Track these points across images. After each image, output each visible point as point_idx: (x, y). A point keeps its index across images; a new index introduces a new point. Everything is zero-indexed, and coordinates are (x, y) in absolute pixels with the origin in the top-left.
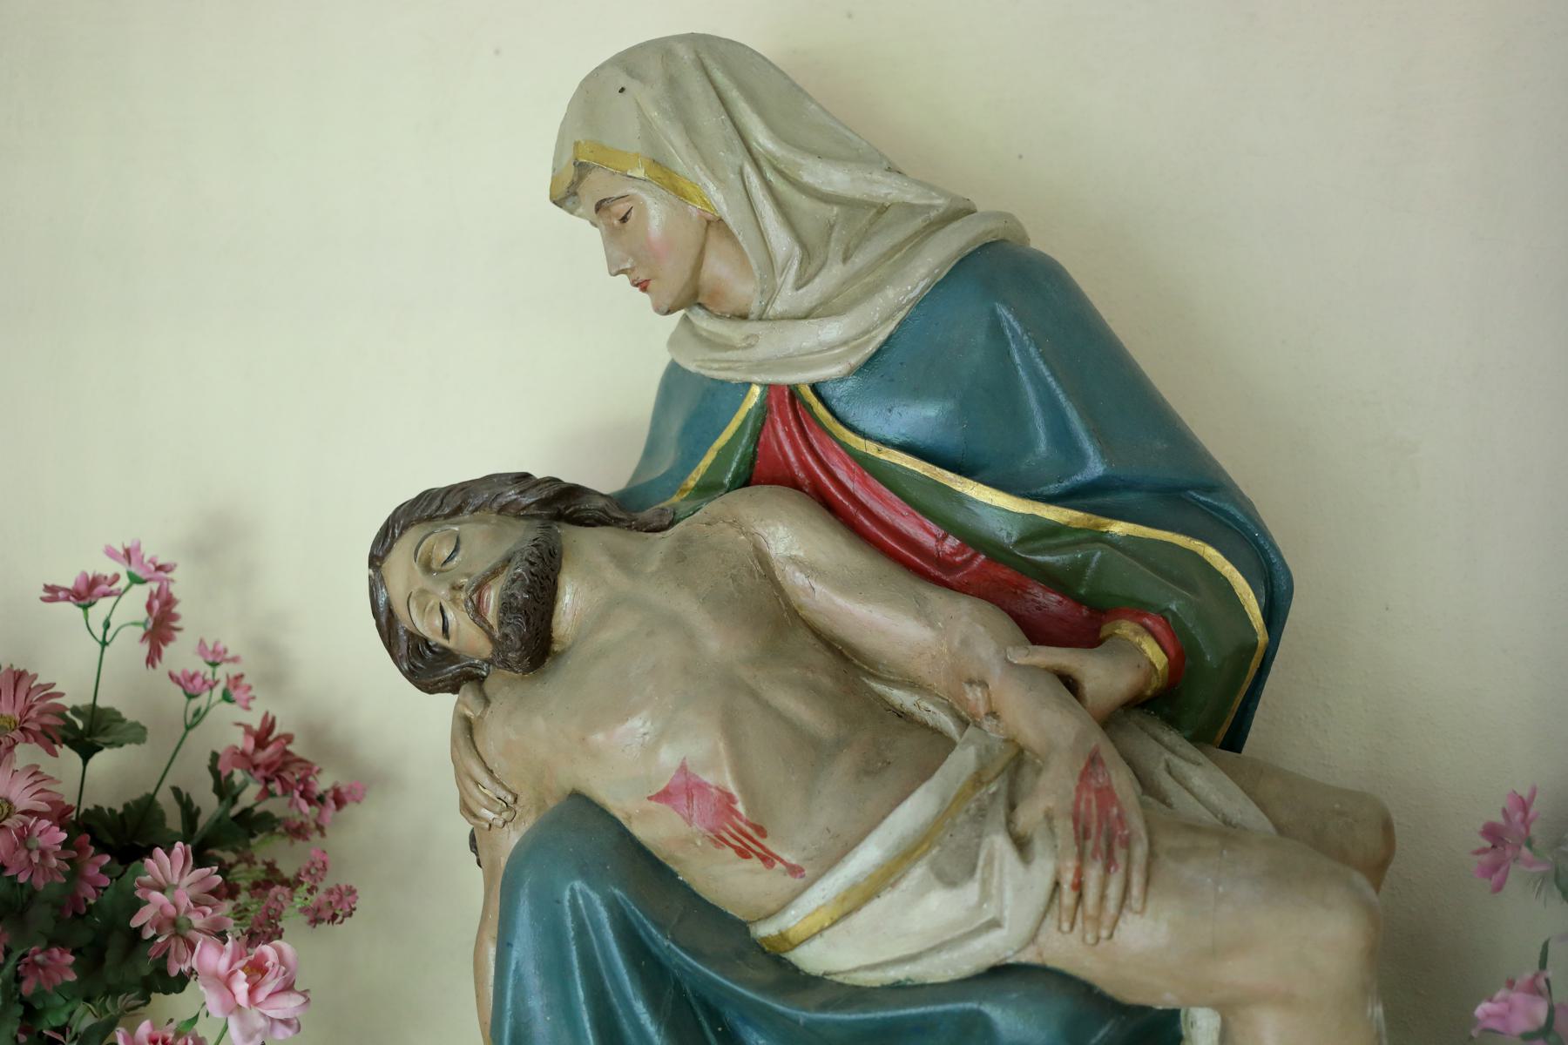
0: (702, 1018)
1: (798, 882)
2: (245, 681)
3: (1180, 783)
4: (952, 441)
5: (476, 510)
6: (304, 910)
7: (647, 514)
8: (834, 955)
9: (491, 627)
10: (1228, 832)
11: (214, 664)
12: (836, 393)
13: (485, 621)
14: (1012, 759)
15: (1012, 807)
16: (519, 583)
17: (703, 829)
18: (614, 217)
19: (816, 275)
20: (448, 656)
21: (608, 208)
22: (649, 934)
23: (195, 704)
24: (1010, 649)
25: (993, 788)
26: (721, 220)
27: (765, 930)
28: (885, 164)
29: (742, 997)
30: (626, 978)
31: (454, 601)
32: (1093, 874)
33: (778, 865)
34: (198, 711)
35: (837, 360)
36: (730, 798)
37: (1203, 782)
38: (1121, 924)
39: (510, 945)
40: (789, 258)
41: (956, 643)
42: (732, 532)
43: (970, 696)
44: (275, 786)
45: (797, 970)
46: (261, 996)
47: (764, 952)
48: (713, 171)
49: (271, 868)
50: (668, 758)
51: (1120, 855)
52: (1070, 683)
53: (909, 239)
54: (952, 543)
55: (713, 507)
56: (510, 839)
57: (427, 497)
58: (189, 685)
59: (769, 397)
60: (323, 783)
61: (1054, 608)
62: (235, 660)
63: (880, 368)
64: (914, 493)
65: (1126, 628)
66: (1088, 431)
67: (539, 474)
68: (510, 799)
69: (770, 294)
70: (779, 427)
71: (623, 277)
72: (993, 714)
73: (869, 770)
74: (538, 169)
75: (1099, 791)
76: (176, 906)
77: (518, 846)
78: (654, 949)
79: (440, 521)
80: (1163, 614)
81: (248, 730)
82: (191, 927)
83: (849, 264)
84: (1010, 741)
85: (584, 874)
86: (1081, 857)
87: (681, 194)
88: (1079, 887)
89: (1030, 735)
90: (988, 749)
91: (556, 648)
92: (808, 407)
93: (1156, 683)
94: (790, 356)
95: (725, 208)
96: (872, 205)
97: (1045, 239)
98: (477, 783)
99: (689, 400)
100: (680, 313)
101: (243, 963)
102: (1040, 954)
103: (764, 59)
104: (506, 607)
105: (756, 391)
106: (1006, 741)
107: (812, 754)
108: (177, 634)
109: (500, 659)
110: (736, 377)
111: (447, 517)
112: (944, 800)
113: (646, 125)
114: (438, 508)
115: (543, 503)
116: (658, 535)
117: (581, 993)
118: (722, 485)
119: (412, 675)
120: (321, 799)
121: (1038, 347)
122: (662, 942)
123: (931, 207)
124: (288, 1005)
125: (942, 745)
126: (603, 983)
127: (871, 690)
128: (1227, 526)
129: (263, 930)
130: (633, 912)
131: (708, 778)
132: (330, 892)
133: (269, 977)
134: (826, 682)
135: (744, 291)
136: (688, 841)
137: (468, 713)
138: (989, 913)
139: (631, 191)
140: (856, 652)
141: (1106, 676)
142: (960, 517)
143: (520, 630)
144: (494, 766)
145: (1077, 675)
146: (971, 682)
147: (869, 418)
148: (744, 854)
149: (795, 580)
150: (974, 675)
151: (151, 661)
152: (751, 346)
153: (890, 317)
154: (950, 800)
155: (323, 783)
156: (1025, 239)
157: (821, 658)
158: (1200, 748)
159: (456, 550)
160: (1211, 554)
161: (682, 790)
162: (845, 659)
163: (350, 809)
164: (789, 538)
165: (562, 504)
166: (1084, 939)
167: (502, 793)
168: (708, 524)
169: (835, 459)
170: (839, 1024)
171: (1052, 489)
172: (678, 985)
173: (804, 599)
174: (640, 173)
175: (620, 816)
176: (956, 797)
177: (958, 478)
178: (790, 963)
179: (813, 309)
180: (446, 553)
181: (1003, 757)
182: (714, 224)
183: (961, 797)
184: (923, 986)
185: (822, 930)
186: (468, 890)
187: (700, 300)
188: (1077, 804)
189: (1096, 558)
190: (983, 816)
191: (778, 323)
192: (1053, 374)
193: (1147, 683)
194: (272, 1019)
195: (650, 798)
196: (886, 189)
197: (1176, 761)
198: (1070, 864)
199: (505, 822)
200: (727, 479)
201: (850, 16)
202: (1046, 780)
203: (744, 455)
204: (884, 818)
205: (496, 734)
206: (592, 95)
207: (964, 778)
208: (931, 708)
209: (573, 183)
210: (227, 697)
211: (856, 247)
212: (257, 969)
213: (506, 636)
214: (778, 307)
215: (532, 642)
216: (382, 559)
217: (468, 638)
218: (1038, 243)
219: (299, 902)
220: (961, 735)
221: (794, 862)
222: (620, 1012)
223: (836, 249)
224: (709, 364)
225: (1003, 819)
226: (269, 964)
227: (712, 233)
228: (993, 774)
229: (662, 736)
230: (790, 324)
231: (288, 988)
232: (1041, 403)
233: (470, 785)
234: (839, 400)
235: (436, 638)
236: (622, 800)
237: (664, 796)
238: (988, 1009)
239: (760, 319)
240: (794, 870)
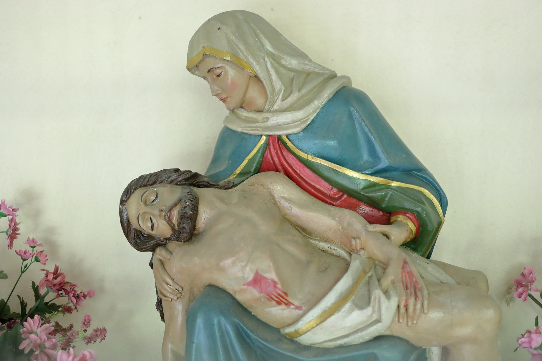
1: (301, 312)
2: (44, 253)
4: (335, 154)
6: (84, 338)
8: (317, 337)
9: (174, 225)
11: (33, 247)
13: (172, 223)
18: (213, 75)
20: (150, 237)
21: (213, 71)
23: (25, 263)
27: (288, 330)
32: (411, 301)
34: (27, 265)
35: (297, 126)
40: (280, 90)
45: (300, 344)
51: (419, 294)
52: (387, 236)
55: (252, 179)
57: (142, 178)
58: (24, 256)
59: (269, 140)
62: (40, 245)
63: (309, 129)
65: (401, 218)
67: (182, 169)
68: (180, 289)
70: (272, 150)
75: (408, 273)
76: (40, 339)
82: (45, 348)
84: (370, 258)
85: (222, 313)
86: (407, 295)
93: (412, 236)
98: (167, 284)
99: (230, 141)
102: (391, 331)
105: (264, 138)
108: (18, 236)
111: (150, 185)
113: (229, 41)
115: (186, 180)
118: (250, 172)
144: (175, 277)
148: (279, 303)
149: (285, 204)
151: (10, 246)
152: (264, 122)
153: (315, 112)
159: (157, 197)
160: (426, 192)
162: (304, 231)
164: (281, 189)
165: (192, 180)
173: (287, 211)
174: (229, 58)
175: (231, 292)
177: (341, 167)
179: (287, 108)
184: (351, 346)
198: (404, 298)
199: (178, 298)
201: (272, 9)
210: (37, 260)
214: (275, 107)
215: (187, 231)
216: (126, 201)
217: (162, 229)
221: (298, 305)
223: (295, 87)
224: (246, 129)
238: (376, 351)
240: (298, 308)
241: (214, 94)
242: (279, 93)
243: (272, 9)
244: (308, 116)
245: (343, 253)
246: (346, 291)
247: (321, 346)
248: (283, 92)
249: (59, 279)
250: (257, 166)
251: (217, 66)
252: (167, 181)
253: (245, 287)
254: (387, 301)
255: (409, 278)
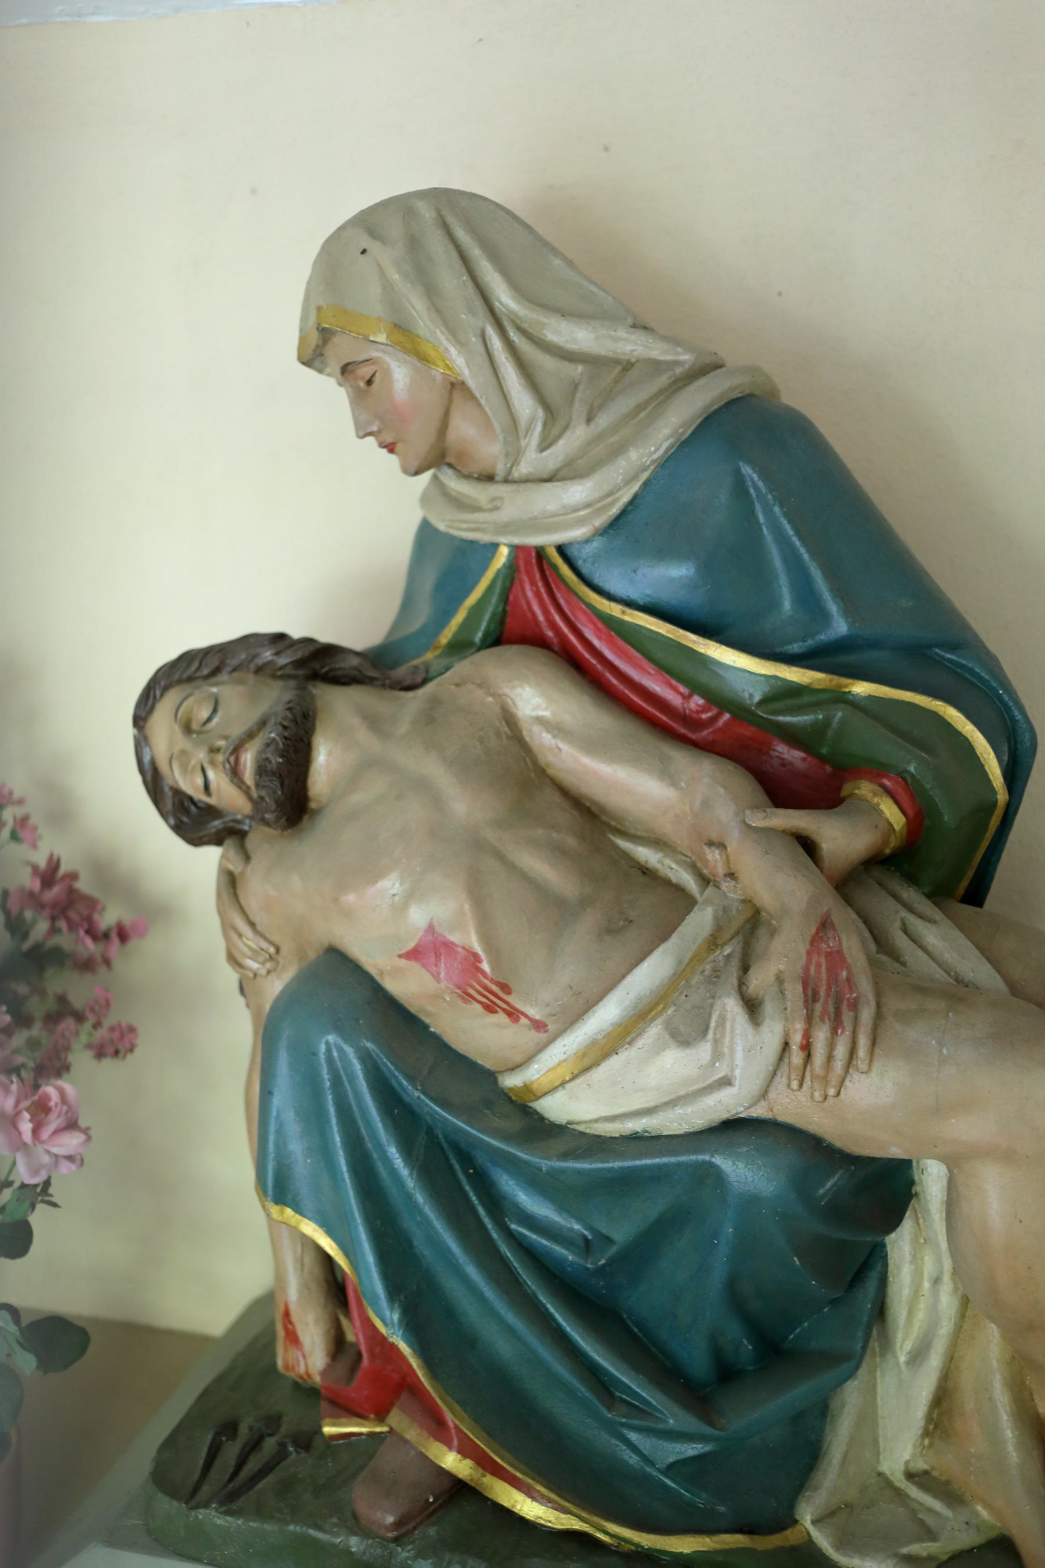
0: (454, 1162)
1: (542, 1036)
3: (914, 941)
4: (694, 601)
5: (235, 670)
6: (89, 1046)
7: (401, 672)
8: (570, 1106)
9: (248, 788)
10: (957, 993)
12: (583, 556)
13: (243, 782)
14: (748, 921)
15: (745, 969)
16: (273, 747)
17: (451, 986)
18: (360, 380)
19: (560, 436)
20: (211, 812)
21: (353, 372)
22: (401, 1084)
24: (748, 812)
25: (727, 950)
26: (463, 383)
27: (511, 1081)
28: (630, 321)
29: (488, 1145)
30: (380, 1125)
31: (212, 763)
32: (821, 1036)
33: (523, 1020)
35: (581, 522)
36: (476, 958)
37: (939, 941)
38: (847, 1083)
39: (270, 1093)
40: (532, 420)
41: (697, 804)
42: (479, 693)
43: (710, 857)
44: (62, 924)
45: (542, 1118)
46: (45, 1134)
47: (512, 1101)
48: (453, 332)
49: (62, 1000)
50: (418, 917)
51: (847, 1017)
52: (808, 846)
53: (655, 397)
54: (697, 701)
55: (463, 667)
56: (275, 987)
57: (187, 658)
59: (516, 558)
60: (107, 919)
61: (801, 765)
62: (21, 802)
64: (659, 655)
65: (865, 789)
66: (831, 590)
67: (296, 633)
68: (272, 950)
69: (515, 455)
71: (371, 440)
72: (731, 875)
73: (611, 930)
74: (287, 331)
75: (828, 955)
77: (283, 992)
78: (406, 1099)
79: (199, 682)
80: (903, 776)
81: (35, 868)
83: (593, 426)
84: (747, 902)
85: (338, 1028)
86: (809, 1019)
87: (423, 358)
88: (807, 1048)
89: (766, 899)
90: (725, 910)
91: (313, 805)
92: (555, 568)
93: (894, 843)
94: (535, 518)
95: (466, 372)
96: (616, 362)
97: (793, 395)
98: (240, 935)
99: (442, 560)
100: (427, 476)
101: (25, 1104)
103: (508, 212)
104: (261, 770)
105: (504, 551)
106: (744, 901)
107: (558, 912)
109: (258, 815)
110: (485, 538)
111: (206, 677)
112: (680, 962)
113: (388, 287)
114: (198, 669)
115: (298, 664)
116: (410, 694)
117: (338, 1139)
119: (179, 829)
120: (106, 936)
121: (782, 506)
122: (413, 1093)
123: (677, 363)
124: (71, 1142)
125: (682, 902)
126: (358, 1130)
127: (617, 848)
128: (973, 684)
129: (54, 1065)
130: (385, 1064)
131: (455, 938)
132: (112, 1029)
133: (52, 1116)
134: (571, 842)
135: (490, 451)
136: (437, 996)
137: (231, 867)
138: (721, 1070)
139: (375, 354)
140: (603, 809)
141: (842, 837)
142: (703, 678)
143: (275, 792)
144: (256, 919)
145: (816, 837)
146: (711, 844)
147: (615, 581)
148: (490, 1009)
149: (543, 740)
150: (714, 837)
152: (497, 508)
153: (635, 478)
154: (686, 961)
155: (107, 919)
156: (774, 392)
157: (564, 816)
158: (936, 904)
159: (215, 711)
161: (429, 950)
162: (593, 819)
163: (133, 943)
164: (536, 699)
165: (316, 664)
166: (812, 1096)
167: (265, 945)
168: (457, 685)
169: (583, 618)
170: (579, 1172)
171: (796, 648)
172: (430, 1132)
173: (551, 758)
174: (382, 338)
175: (373, 972)
176: (691, 960)
178: (537, 1113)
180: (205, 714)
181: (738, 920)
182: (456, 387)
183: (696, 959)
184: (659, 1137)
185: (563, 1084)
186: (232, 1034)
187: (448, 460)
188: (806, 968)
189: (836, 719)
190: (717, 977)
191: (523, 486)
192: (798, 533)
193: (886, 842)
194: (56, 1156)
195: (400, 956)
196: (631, 345)
197: (912, 920)
198: (799, 1026)
199: (269, 972)
200: (478, 636)
201: (606, 149)
202: (778, 944)
203: (494, 615)
204: (623, 977)
205: (257, 889)
206: (333, 260)
207: (700, 940)
208: (674, 866)
209: (317, 346)
211: (600, 407)
212: (41, 1110)
213: (262, 798)
214: (524, 469)
215: (290, 800)
216: (145, 719)
217: (228, 796)
218: (791, 397)
219: (84, 1038)
220: (702, 893)
221: (537, 1017)
222: (375, 1156)
223: (579, 409)
225: (735, 982)
226: (52, 1104)
227: (457, 396)
228: (729, 936)
229: (411, 896)
230: (534, 487)
231: (72, 1125)
232: (785, 561)
233: (234, 937)
234: (585, 561)
235: (200, 796)
236: (376, 956)
237: (414, 954)
238: (718, 1160)
239: (506, 481)
240: (538, 1026)
241: (361, 434)
242: (528, 430)
243: (606, 149)
244: (610, 494)
245: (688, 880)
246: (652, 992)
247: (588, 1131)
248: (539, 427)
249: (56, 892)
250: (488, 626)
251: (360, 359)
252: (248, 668)
253: (403, 962)
254: (749, 1030)
255: (828, 970)
